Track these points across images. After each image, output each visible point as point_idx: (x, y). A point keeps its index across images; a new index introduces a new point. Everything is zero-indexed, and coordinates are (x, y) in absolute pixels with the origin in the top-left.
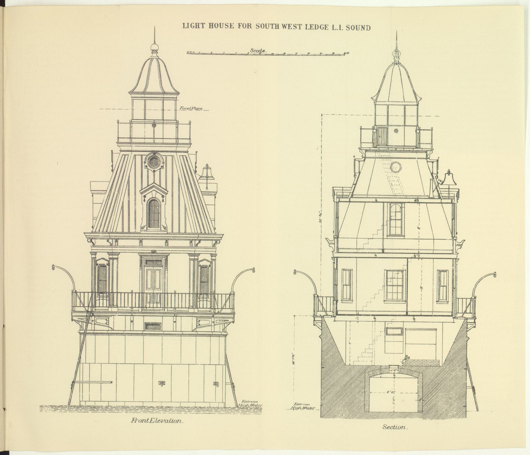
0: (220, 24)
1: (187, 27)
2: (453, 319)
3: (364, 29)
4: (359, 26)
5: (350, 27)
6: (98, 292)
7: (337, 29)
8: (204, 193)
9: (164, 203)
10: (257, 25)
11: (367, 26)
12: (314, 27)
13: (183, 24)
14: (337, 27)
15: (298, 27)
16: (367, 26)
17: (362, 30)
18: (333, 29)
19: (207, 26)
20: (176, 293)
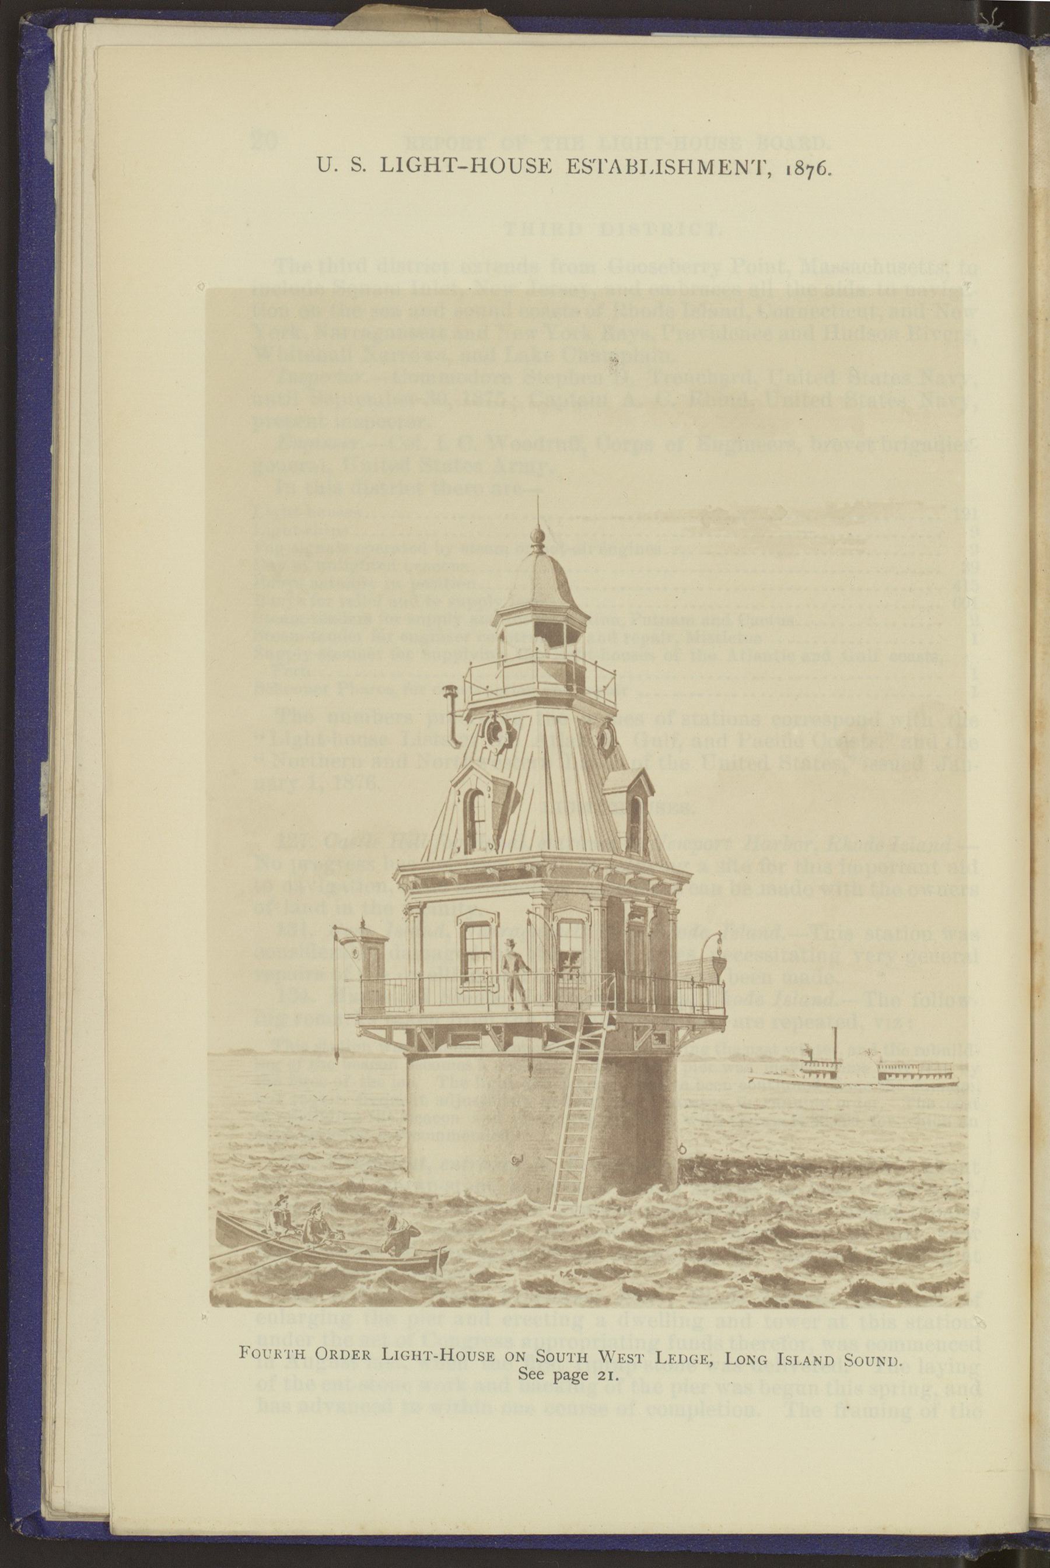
0: (558, 1354)
1: (395, 1358)
2: (727, 1014)
3: (820, 1363)
4: (873, 1358)
5: (515, 1358)
6: (669, 979)
7: (277, 1356)
8: (496, 712)
9: (457, 845)
10: (538, 1354)
11: (827, 1357)
12: (677, 1359)
13: (726, 1355)
14: (801, 1360)
15: (636, 1359)
16: (827, 1357)
17: (878, 1365)
18: (728, 1363)
19: (310, 1353)
20: (525, 1063)
